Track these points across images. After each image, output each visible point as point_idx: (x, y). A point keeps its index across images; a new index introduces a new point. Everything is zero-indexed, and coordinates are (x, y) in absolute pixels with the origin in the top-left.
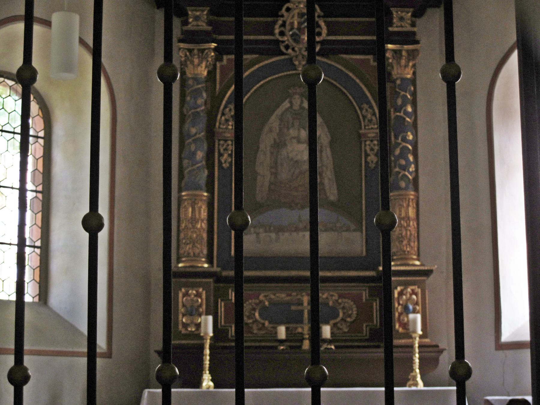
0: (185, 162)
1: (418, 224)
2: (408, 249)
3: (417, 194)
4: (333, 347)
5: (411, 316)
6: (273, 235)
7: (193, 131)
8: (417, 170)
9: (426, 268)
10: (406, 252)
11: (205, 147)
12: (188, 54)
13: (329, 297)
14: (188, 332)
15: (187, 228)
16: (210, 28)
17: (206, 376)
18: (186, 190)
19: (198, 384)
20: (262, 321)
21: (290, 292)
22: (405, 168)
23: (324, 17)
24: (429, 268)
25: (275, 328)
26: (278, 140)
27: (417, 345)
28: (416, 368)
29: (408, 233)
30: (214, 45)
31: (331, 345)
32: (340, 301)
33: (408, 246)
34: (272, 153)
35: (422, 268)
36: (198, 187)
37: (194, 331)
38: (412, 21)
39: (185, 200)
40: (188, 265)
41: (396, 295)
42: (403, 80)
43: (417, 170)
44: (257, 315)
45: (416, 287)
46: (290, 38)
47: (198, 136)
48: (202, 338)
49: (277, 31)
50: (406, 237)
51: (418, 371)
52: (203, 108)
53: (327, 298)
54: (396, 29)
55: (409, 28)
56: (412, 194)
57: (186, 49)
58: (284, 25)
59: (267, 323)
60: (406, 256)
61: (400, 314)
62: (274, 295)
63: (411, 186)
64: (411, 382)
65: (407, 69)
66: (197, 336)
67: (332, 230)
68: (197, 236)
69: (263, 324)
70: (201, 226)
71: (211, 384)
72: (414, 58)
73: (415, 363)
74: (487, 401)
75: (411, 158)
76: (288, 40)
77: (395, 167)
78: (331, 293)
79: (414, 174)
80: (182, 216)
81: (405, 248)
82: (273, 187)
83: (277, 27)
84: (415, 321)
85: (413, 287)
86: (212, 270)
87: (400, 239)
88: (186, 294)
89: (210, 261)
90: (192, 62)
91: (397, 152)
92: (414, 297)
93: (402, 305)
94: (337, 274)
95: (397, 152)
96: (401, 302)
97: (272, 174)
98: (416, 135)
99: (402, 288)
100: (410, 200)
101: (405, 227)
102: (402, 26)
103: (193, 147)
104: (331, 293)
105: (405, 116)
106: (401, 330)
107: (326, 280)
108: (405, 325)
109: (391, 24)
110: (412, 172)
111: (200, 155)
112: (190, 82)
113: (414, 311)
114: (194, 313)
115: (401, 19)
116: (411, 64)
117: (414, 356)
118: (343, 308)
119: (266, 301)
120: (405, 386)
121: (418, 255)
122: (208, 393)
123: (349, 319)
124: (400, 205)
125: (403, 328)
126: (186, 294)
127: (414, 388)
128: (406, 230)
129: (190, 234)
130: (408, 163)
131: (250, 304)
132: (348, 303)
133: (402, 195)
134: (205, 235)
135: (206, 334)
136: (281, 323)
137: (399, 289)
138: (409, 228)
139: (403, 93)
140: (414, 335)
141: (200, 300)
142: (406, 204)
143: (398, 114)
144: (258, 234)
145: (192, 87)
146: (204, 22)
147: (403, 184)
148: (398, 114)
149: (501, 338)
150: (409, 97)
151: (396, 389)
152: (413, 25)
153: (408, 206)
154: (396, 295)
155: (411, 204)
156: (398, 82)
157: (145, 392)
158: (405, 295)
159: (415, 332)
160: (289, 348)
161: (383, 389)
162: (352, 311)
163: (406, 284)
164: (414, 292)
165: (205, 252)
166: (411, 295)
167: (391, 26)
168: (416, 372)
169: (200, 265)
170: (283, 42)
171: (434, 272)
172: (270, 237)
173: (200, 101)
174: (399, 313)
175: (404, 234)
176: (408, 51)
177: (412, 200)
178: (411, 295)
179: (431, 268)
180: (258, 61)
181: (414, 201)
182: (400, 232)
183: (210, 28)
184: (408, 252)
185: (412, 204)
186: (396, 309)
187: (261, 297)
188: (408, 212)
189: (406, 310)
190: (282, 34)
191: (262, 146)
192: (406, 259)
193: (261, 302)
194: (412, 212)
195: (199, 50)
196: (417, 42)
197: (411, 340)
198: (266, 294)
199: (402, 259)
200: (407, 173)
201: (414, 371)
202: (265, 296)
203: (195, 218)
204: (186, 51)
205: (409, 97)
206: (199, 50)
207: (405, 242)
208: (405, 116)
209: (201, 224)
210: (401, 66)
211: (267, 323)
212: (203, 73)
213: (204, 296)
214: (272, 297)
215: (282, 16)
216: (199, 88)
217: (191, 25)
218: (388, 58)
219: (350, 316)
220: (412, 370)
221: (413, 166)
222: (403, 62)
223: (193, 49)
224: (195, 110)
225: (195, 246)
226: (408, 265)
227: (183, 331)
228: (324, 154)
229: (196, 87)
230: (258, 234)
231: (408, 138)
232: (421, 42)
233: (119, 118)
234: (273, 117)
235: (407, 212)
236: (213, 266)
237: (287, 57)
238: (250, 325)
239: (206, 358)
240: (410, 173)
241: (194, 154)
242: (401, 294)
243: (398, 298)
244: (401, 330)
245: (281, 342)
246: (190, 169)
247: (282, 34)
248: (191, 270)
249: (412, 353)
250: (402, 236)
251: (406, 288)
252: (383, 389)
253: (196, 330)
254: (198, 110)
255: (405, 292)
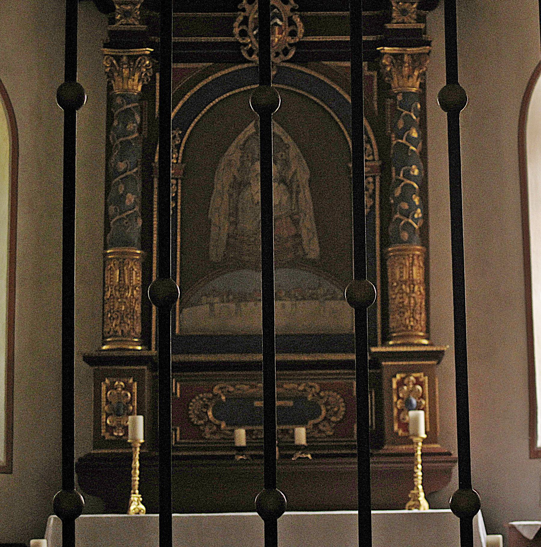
0: (112, 208)
1: (427, 290)
2: (412, 323)
3: (424, 249)
4: (309, 456)
5: (411, 413)
6: (233, 306)
7: (122, 166)
8: (425, 215)
9: (434, 349)
10: (409, 328)
11: (139, 187)
12: (114, 62)
13: (309, 390)
14: (113, 438)
15: (114, 298)
16: (144, 27)
17: (134, 497)
18: (113, 245)
19: (125, 509)
20: (217, 422)
21: (254, 383)
22: (407, 214)
23: (298, 10)
24: (439, 349)
25: (233, 431)
26: (239, 179)
27: (419, 453)
28: (418, 484)
29: (412, 301)
30: (149, 50)
31: (306, 454)
32: (322, 394)
33: (412, 319)
34: (231, 195)
35: (429, 349)
36: (128, 243)
37: (122, 436)
38: (417, 15)
39: (111, 259)
40: (114, 347)
41: (394, 386)
42: (406, 94)
43: (425, 215)
44: (210, 413)
45: (422, 374)
46: (254, 39)
47: (128, 173)
48: (130, 446)
49: (236, 31)
50: (410, 306)
51: (420, 487)
52: (136, 135)
53: (305, 390)
54: (395, 26)
55: (413, 25)
56: (417, 249)
57: (112, 56)
58: (245, 21)
59: (223, 425)
60: (411, 333)
61: (400, 411)
62: (234, 386)
63: (417, 237)
64: (411, 503)
65: (411, 80)
66: (122, 442)
67: (312, 297)
68: (126, 308)
69: (219, 426)
70: (132, 295)
71: (142, 507)
72: (421, 66)
73: (417, 477)
74: (513, 527)
75: (417, 200)
76: (251, 42)
77: (396, 213)
78: (310, 384)
79: (421, 222)
80: (108, 282)
81: (407, 321)
82: (232, 240)
83: (236, 24)
84: (416, 420)
85: (418, 375)
86: (146, 353)
87: (401, 311)
88: (111, 387)
89: (145, 340)
90: (120, 74)
91: (398, 192)
92: (419, 387)
93: (403, 399)
94: (319, 357)
95: (398, 192)
96: (401, 395)
97: (231, 223)
98: (425, 170)
99: (403, 375)
100: (415, 257)
101: (407, 294)
102: (403, 22)
103: (121, 189)
104: (310, 384)
105: (408, 144)
106: (400, 432)
107: (284, 366)
108: (405, 426)
109: (389, 20)
110: (418, 218)
111: (130, 199)
112: (119, 101)
113: (418, 408)
114: (122, 411)
115: (404, 12)
116: (416, 73)
117: (415, 467)
118: (326, 404)
119: (222, 395)
120: (404, 509)
121: (428, 331)
122: (137, 520)
123: (333, 419)
124: (401, 263)
125: (404, 431)
126: (111, 387)
127: (415, 511)
128: (409, 297)
129: (117, 305)
130: (413, 207)
131: (202, 399)
132: (335, 397)
133: (405, 250)
134: (138, 308)
135: (135, 440)
136: (240, 426)
137: (398, 376)
138: (414, 295)
139: (406, 112)
140: (415, 439)
141: (129, 395)
142: (409, 264)
143: (400, 141)
144: (212, 305)
145: (121, 107)
146: (137, 19)
147: (405, 236)
148: (400, 141)
149: (536, 443)
150: (414, 117)
151: (373, 512)
152: (421, 19)
153: (412, 264)
154: (394, 386)
155: (416, 262)
156: (399, 98)
157: (50, 519)
158: (405, 385)
159: (417, 435)
160: (249, 458)
161: (357, 512)
162: (339, 407)
163: (408, 371)
164: (418, 382)
165: (138, 329)
166: (414, 385)
167: (389, 22)
168: (418, 489)
169: (131, 347)
170: (246, 45)
171: (445, 353)
172: (228, 307)
173: (131, 126)
174: (398, 410)
175: (406, 302)
176: (412, 55)
177: (418, 256)
178: (414, 385)
179: (442, 349)
180: (205, 74)
181: (420, 258)
182: (401, 300)
183: (144, 27)
184: (412, 326)
185: (419, 263)
186: (394, 405)
187: (216, 390)
188: (412, 274)
189: (408, 405)
190: (243, 34)
191: (218, 187)
192: (408, 336)
193: (215, 396)
194: (417, 274)
195: (129, 57)
196: (428, 44)
197: (411, 447)
198: (222, 385)
199: (402, 337)
200: (410, 221)
201: (415, 488)
202: (221, 388)
203: (124, 284)
204: (111, 58)
205: (414, 117)
206: (129, 57)
207: (407, 314)
208: (408, 144)
209: (132, 292)
210: (403, 77)
211: (223, 425)
212: (135, 87)
213: (135, 390)
214: (231, 389)
215: (244, 10)
216: (130, 108)
217: (120, 23)
218: (385, 66)
219: (336, 413)
220: (413, 486)
221: (419, 210)
222: (406, 70)
223: (122, 56)
224: (124, 139)
225: (124, 322)
226: (413, 345)
227: (108, 437)
228: (301, 195)
229: (126, 107)
230: (212, 305)
231: (412, 173)
232: (433, 44)
233: (22, 150)
234: (232, 148)
235: (410, 274)
236: (150, 349)
237: (251, 65)
238: (201, 428)
239: (135, 473)
240: (416, 221)
241: (123, 196)
242: (401, 383)
243: (398, 388)
244: (400, 432)
245: (240, 449)
246: (118, 217)
247: (243, 34)
248: (115, 354)
249: (413, 463)
250: (403, 306)
251: (408, 376)
252: (357, 512)
253: (124, 435)
254: (129, 138)
255: (406, 381)
